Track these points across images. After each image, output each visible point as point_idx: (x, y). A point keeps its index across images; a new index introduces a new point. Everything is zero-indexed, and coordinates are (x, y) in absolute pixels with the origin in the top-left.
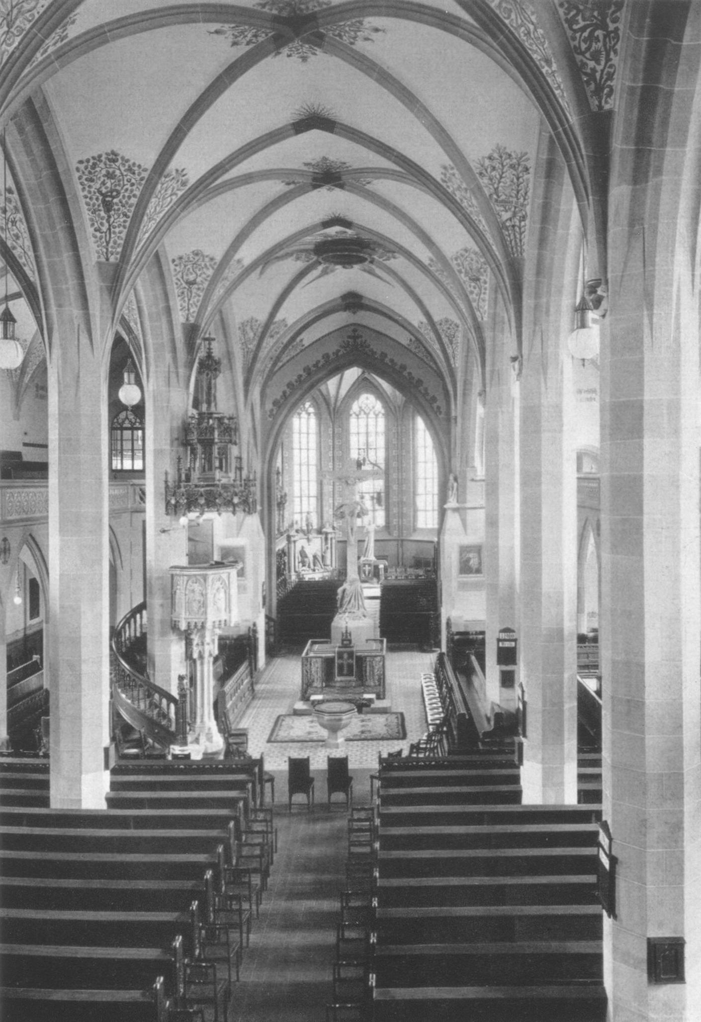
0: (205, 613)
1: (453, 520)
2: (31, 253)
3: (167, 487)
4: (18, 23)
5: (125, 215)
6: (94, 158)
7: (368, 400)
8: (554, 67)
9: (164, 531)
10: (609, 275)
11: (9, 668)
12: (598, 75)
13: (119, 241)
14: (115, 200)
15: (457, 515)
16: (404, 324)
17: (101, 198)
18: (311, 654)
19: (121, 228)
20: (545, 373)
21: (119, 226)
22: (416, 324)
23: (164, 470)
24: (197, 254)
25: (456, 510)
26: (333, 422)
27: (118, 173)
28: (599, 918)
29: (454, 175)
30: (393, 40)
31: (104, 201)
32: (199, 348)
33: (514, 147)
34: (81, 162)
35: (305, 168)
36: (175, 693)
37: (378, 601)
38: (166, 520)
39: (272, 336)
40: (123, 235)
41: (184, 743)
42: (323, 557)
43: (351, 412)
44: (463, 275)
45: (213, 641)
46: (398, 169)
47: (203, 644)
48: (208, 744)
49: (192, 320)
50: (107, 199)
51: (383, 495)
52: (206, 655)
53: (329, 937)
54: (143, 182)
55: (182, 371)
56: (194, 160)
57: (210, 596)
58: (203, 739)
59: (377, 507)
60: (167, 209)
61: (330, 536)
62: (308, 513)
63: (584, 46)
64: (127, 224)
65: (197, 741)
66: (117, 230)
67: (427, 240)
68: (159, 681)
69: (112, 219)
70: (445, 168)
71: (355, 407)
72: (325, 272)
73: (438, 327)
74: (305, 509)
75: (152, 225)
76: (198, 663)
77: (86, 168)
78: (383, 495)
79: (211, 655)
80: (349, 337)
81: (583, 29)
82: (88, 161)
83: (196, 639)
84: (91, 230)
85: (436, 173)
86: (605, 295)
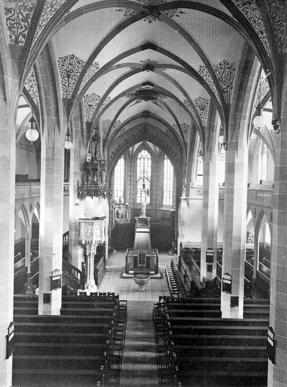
0: (92, 237)
1: (183, 204)
2: (37, 94)
3: (78, 187)
4: (55, 7)
5: (75, 79)
6: (65, 57)
7: (144, 153)
8: (265, 35)
9: (77, 205)
10: (282, 117)
11: (15, 255)
12: (282, 40)
13: (72, 90)
14: (72, 74)
15: (185, 201)
16: (166, 124)
17: (66, 73)
18: (129, 255)
19: (73, 85)
20: (237, 150)
21: (73, 84)
22: (171, 124)
23: (77, 180)
24: (94, 95)
25: (185, 199)
26: (131, 162)
27: (74, 63)
28: (267, 363)
29: (204, 70)
30: (187, 17)
31: (67, 74)
32: (92, 132)
33: (230, 60)
34: (60, 58)
35: (141, 63)
36: (80, 268)
37: (136, 231)
38: (78, 201)
39: (114, 127)
40: (74, 88)
41: (84, 289)
42: (126, 215)
43: (138, 157)
44: (198, 108)
45: (94, 249)
46: (181, 66)
47: (91, 250)
48: (92, 289)
49: (90, 121)
50: (69, 73)
51: (149, 191)
52: (92, 254)
53: (155, 367)
54: (83, 67)
55: (85, 141)
56: (102, 60)
57: (94, 231)
58: (89, 287)
59: (147, 196)
60: (90, 78)
61: (128, 207)
62: (120, 197)
63: (277, 28)
64: (75, 83)
65: (87, 288)
66: (71, 85)
67: (185, 94)
68: (73, 264)
69: (69, 82)
70: (201, 67)
71: (139, 155)
72: (137, 102)
73: (181, 126)
74: (119, 196)
75: (85, 83)
76: (88, 257)
77: (62, 61)
78: (149, 191)
79: (93, 254)
80: (143, 128)
81: (278, 21)
82: (63, 58)
83: (87, 247)
84: (61, 85)
85: (197, 69)
86: (279, 125)
